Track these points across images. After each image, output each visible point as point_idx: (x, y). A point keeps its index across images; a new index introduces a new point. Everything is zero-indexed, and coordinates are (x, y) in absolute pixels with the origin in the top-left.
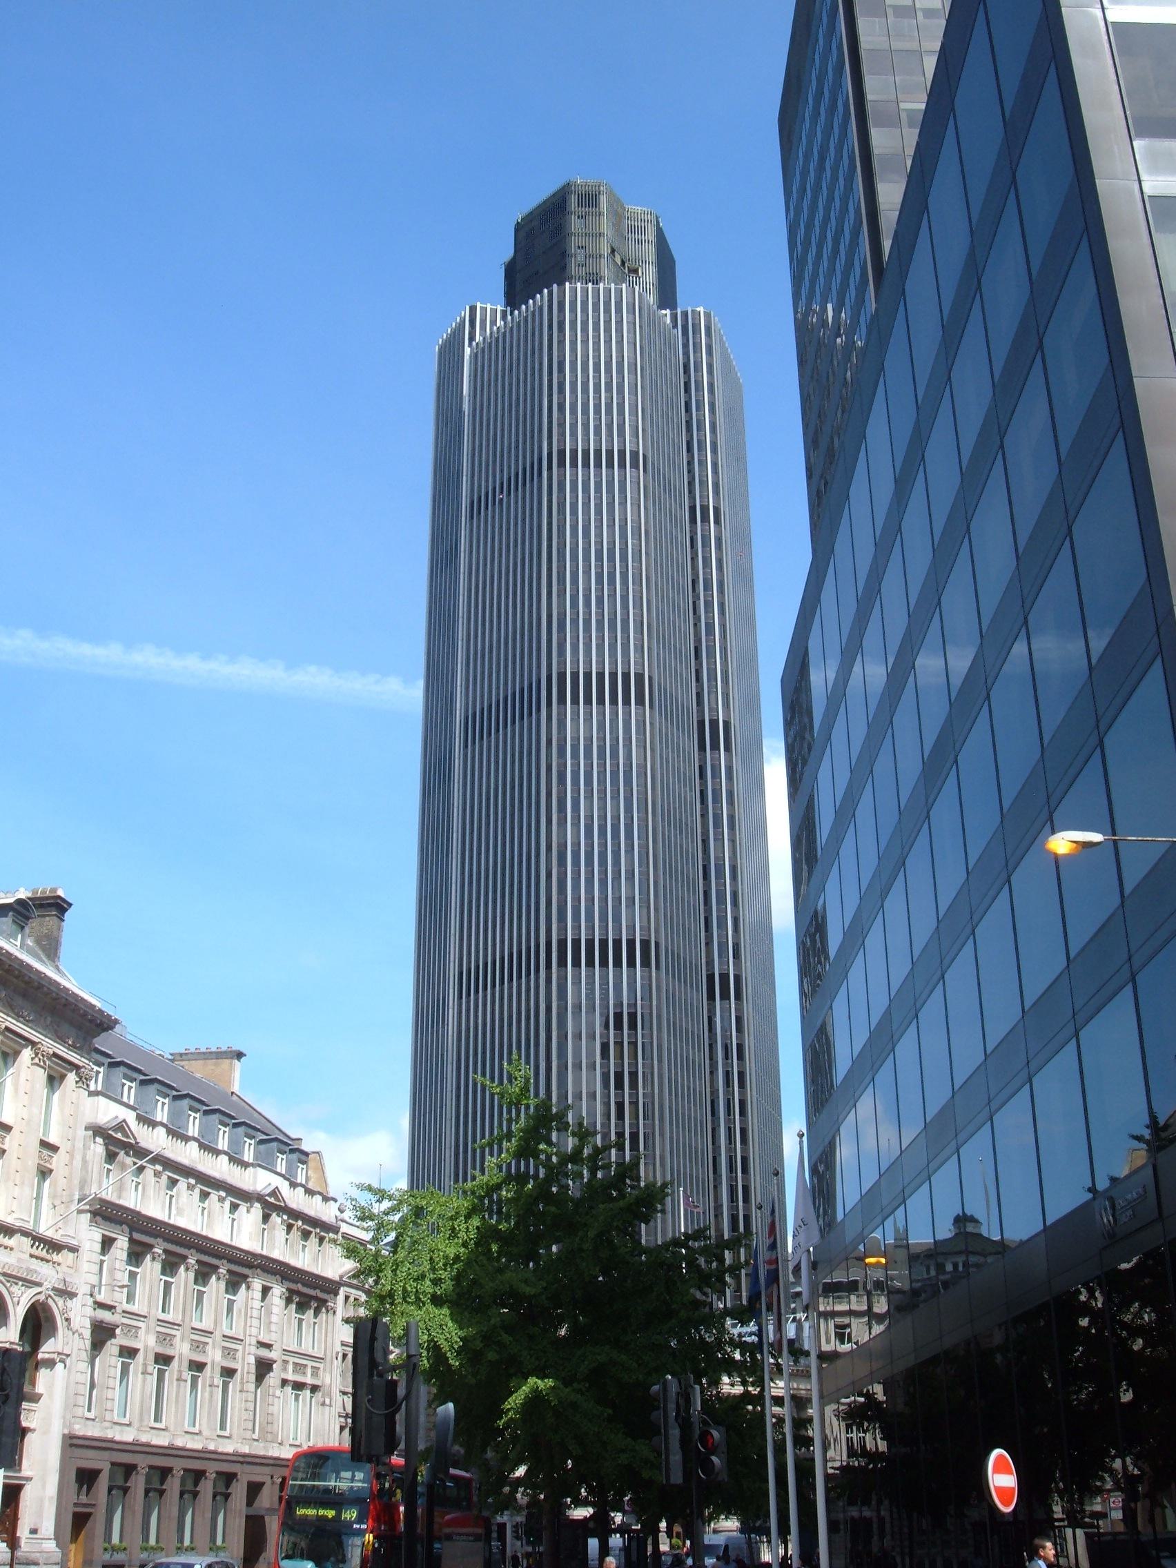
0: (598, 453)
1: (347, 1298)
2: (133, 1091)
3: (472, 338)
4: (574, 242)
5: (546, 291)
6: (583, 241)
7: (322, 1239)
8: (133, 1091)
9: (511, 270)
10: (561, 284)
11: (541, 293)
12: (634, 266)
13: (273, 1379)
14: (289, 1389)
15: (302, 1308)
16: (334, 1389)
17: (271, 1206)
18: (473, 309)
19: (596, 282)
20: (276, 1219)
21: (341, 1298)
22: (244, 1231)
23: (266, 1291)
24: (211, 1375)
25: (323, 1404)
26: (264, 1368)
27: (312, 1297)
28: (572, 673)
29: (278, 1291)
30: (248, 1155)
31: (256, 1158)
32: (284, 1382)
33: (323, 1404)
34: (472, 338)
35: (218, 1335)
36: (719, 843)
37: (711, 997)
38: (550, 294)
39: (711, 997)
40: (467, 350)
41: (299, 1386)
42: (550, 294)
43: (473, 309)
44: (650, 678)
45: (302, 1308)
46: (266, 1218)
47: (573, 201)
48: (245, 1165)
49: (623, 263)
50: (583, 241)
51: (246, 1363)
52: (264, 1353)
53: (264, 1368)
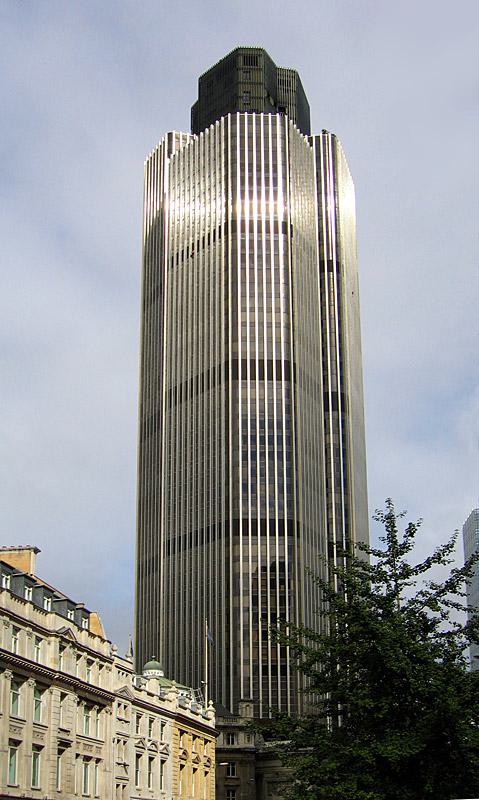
0: (263, 522)
1: (119, 705)
2: (9, 581)
3: (170, 152)
4: (241, 89)
5: (223, 118)
6: (248, 88)
7: (101, 667)
8: (9, 581)
9: (196, 112)
10: (234, 114)
11: (219, 120)
12: (282, 105)
13: (69, 753)
14: (80, 760)
15: (88, 708)
16: (111, 762)
17: (65, 640)
18: (170, 135)
19: (258, 112)
20: (68, 649)
21: (115, 704)
22: (46, 655)
23: (63, 696)
24: (26, 748)
25: (105, 770)
26: (64, 745)
27: (96, 703)
28: (251, 360)
29: (72, 697)
30: (47, 606)
31: (52, 609)
32: (77, 755)
33: (105, 770)
34: (170, 152)
35: (30, 723)
36: (336, 412)
37: (326, 409)
38: (226, 120)
39: (326, 409)
40: (167, 161)
41: (87, 759)
42: (226, 120)
43: (170, 135)
44: (294, 364)
45: (88, 708)
46: (62, 648)
47: (241, 60)
48: (46, 613)
49: (275, 104)
50: (248, 88)
51: (50, 742)
52: (64, 736)
53: (64, 745)
